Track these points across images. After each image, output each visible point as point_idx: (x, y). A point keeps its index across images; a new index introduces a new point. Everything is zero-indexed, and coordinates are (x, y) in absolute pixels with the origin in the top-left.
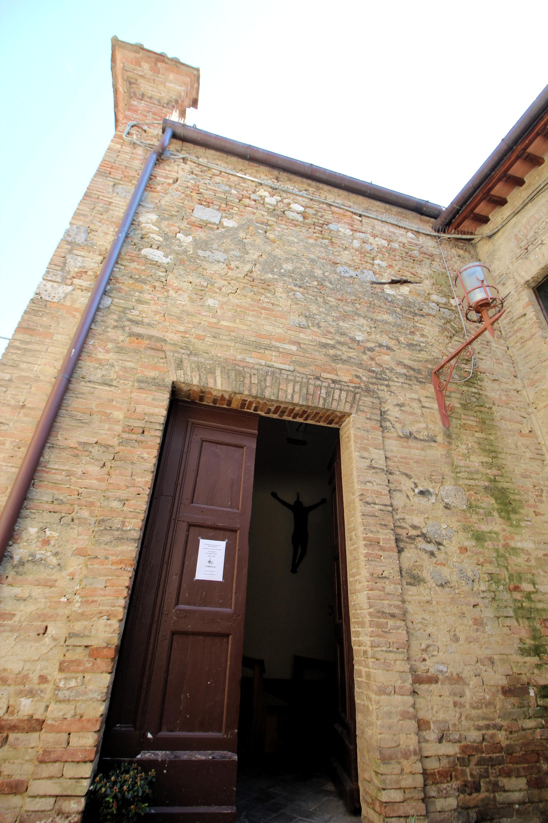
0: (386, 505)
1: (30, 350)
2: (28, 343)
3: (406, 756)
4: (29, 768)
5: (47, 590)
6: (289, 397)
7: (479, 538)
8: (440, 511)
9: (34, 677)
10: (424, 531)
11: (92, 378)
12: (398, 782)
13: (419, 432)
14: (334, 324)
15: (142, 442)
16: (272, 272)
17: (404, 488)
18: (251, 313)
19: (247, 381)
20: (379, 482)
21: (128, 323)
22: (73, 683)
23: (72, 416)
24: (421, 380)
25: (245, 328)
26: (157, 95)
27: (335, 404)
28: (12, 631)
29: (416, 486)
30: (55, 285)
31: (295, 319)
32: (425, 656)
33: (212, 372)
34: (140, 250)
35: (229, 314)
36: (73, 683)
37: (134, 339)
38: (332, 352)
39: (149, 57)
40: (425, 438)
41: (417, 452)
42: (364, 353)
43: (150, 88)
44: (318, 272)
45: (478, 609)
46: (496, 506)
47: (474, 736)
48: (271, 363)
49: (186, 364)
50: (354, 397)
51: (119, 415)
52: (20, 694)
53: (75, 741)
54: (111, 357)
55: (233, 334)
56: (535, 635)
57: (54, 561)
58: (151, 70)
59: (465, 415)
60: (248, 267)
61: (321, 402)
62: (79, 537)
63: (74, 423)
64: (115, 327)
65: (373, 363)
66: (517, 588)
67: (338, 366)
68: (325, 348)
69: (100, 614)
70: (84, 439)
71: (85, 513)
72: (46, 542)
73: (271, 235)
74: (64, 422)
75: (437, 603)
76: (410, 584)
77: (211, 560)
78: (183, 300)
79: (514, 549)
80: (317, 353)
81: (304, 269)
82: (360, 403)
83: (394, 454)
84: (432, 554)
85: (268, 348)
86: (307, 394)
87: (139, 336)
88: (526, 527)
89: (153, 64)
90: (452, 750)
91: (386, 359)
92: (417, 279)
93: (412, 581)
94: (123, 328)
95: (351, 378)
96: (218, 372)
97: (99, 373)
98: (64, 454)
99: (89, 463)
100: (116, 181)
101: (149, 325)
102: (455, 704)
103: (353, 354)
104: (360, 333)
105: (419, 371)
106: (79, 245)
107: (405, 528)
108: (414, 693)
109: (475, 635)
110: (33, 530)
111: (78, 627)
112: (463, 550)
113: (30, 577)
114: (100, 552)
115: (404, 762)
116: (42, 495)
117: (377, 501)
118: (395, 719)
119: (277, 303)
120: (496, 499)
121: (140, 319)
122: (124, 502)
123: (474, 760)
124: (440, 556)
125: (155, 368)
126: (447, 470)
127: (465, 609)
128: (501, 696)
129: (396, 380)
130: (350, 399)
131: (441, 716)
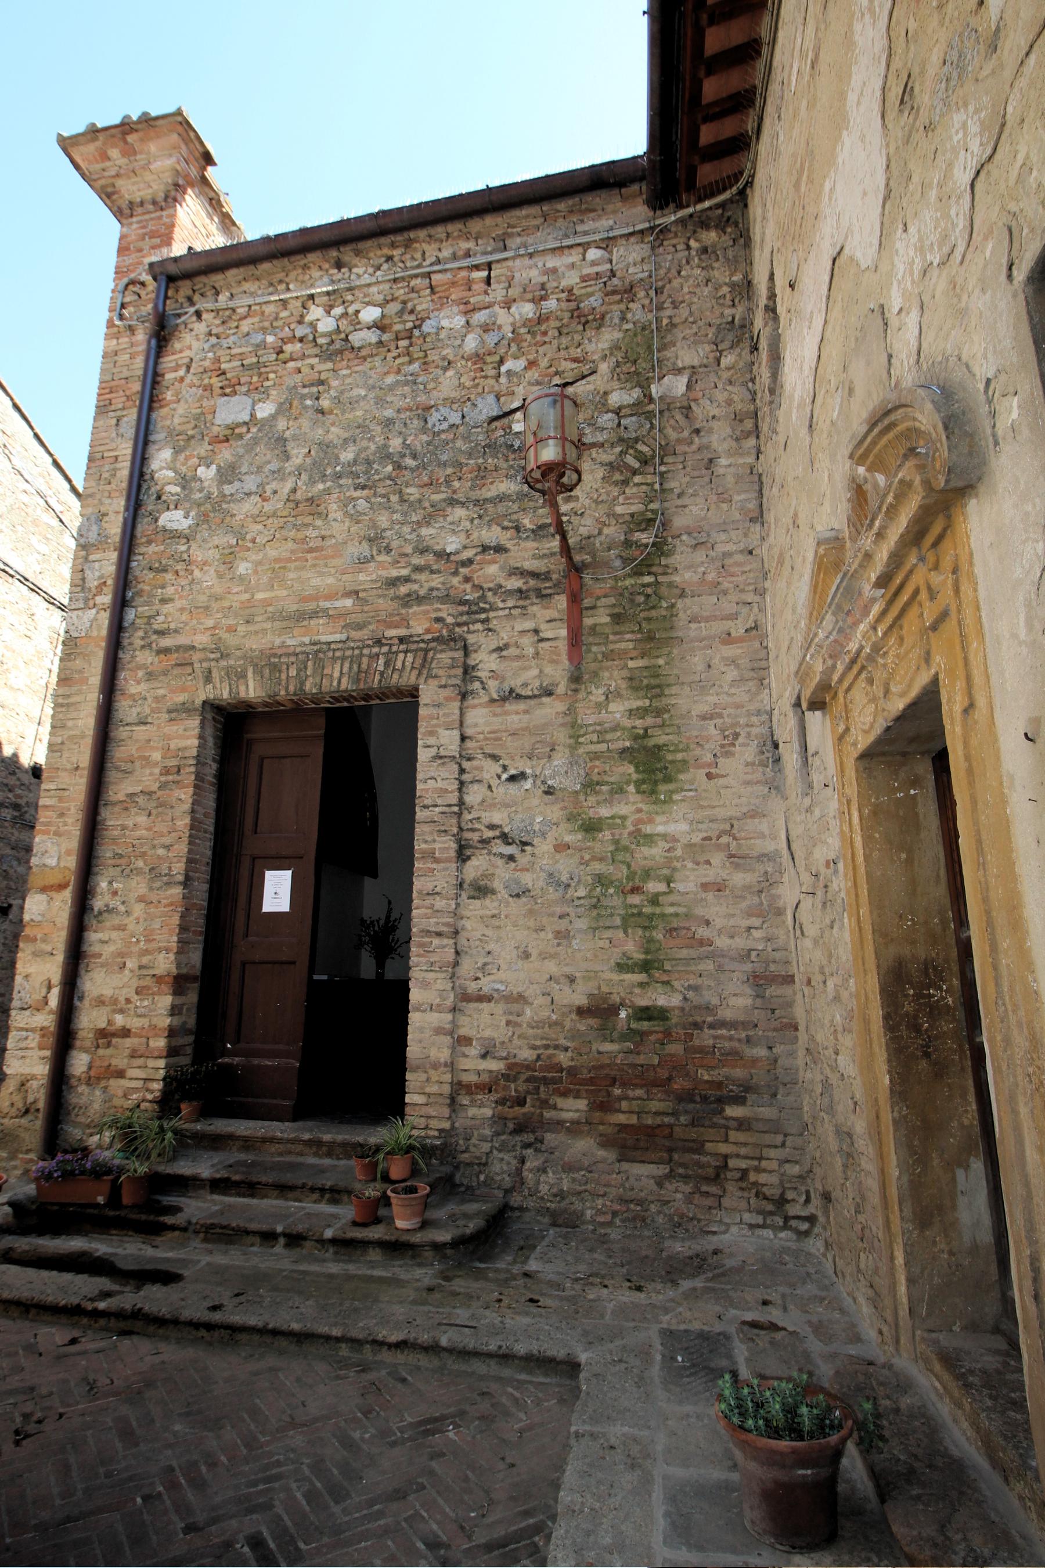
0: (450, 806)
1: (73, 704)
2: (69, 696)
3: (435, 1066)
4: (126, 1061)
5: (121, 933)
6: (335, 683)
7: (591, 828)
8: (537, 799)
9: (122, 999)
10: (506, 830)
11: (129, 720)
12: (422, 1088)
13: (525, 685)
14: (413, 536)
15: (178, 782)
16: (323, 477)
17: (486, 776)
18: (293, 565)
19: (284, 676)
20: (446, 775)
21: (155, 637)
22: (146, 1003)
23: (117, 768)
24: (544, 592)
25: (285, 593)
26: (146, 194)
27: (396, 676)
28: (102, 966)
29: (505, 768)
30: (80, 613)
31: (358, 549)
32: (480, 975)
33: (243, 676)
34: (156, 520)
35: (265, 579)
36: (146, 1003)
37: (162, 656)
38: (403, 590)
39: (113, 136)
40: (536, 692)
41: (516, 718)
42: (456, 573)
43: (135, 188)
44: (395, 444)
45: (566, 921)
46: (635, 776)
47: (526, 1054)
48: (316, 638)
49: (215, 674)
50: (425, 659)
51: (157, 756)
52: (114, 1011)
53: (153, 1043)
54: (142, 687)
55: (270, 609)
56: (648, 945)
57: (122, 908)
58: (123, 156)
59: (615, 634)
60: (289, 485)
61: (377, 677)
62: (139, 886)
63: (120, 775)
64: (143, 647)
65: (468, 587)
66: (635, 890)
67: (411, 611)
68: (394, 585)
69: (160, 950)
70: (131, 790)
71: (140, 863)
72: (115, 893)
73: (325, 403)
74: (112, 775)
75: (506, 917)
76: (473, 898)
77: (277, 891)
78: (208, 579)
79: (646, 836)
80: (381, 601)
81: (373, 447)
82: (433, 665)
83: (479, 730)
84: (511, 858)
85: (314, 614)
86: (359, 671)
87: (166, 651)
88: (683, 800)
89: (122, 144)
90: (495, 1065)
91: (492, 571)
92: (586, 369)
93: (477, 894)
94: (150, 645)
95: (427, 625)
96: (250, 674)
97: (134, 711)
98: (117, 809)
99: (137, 814)
100: (119, 413)
101: (176, 631)
102: (508, 1023)
103: (436, 581)
104: (454, 539)
105: (545, 576)
106: (93, 545)
107: (479, 830)
108: (454, 1010)
109: (552, 950)
110: (104, 885)
111: (145, 960)
112: (561, 847)
113: (108, 924)
114: (153, 897)
115: (432, 1072)
116: (106, 852)
117: (439, 802)
118: (428, 1033)
119: (328, 533)
120: (637, 767)
121: (166, 626)
122: (168, 847)
123: (523, 1077)
124: (523, 860)
125: (183, 690)
126: (561, 736)
127: (545, 920)
128: (574, 1016)
129: (501, 605)
130: (419, 661)
131: (488, 1033)
